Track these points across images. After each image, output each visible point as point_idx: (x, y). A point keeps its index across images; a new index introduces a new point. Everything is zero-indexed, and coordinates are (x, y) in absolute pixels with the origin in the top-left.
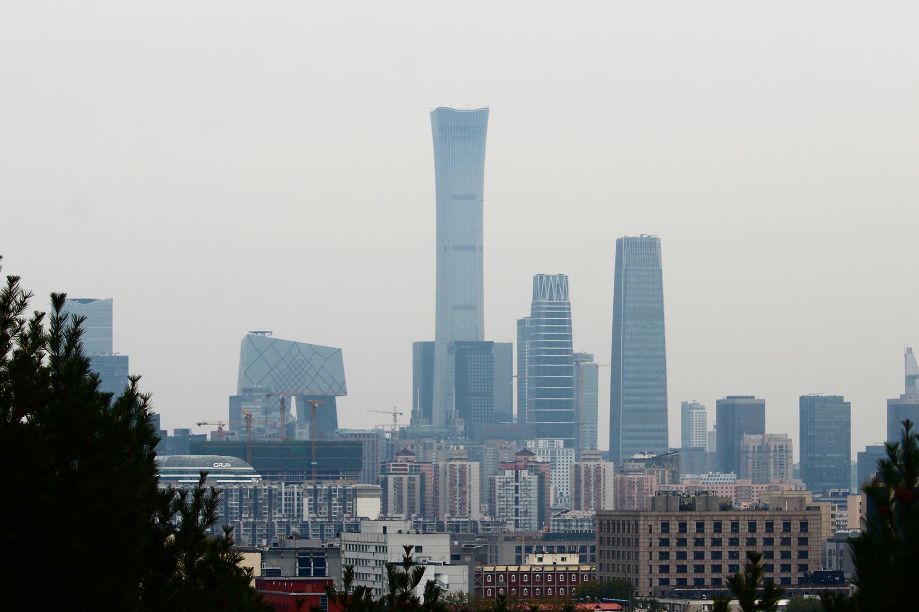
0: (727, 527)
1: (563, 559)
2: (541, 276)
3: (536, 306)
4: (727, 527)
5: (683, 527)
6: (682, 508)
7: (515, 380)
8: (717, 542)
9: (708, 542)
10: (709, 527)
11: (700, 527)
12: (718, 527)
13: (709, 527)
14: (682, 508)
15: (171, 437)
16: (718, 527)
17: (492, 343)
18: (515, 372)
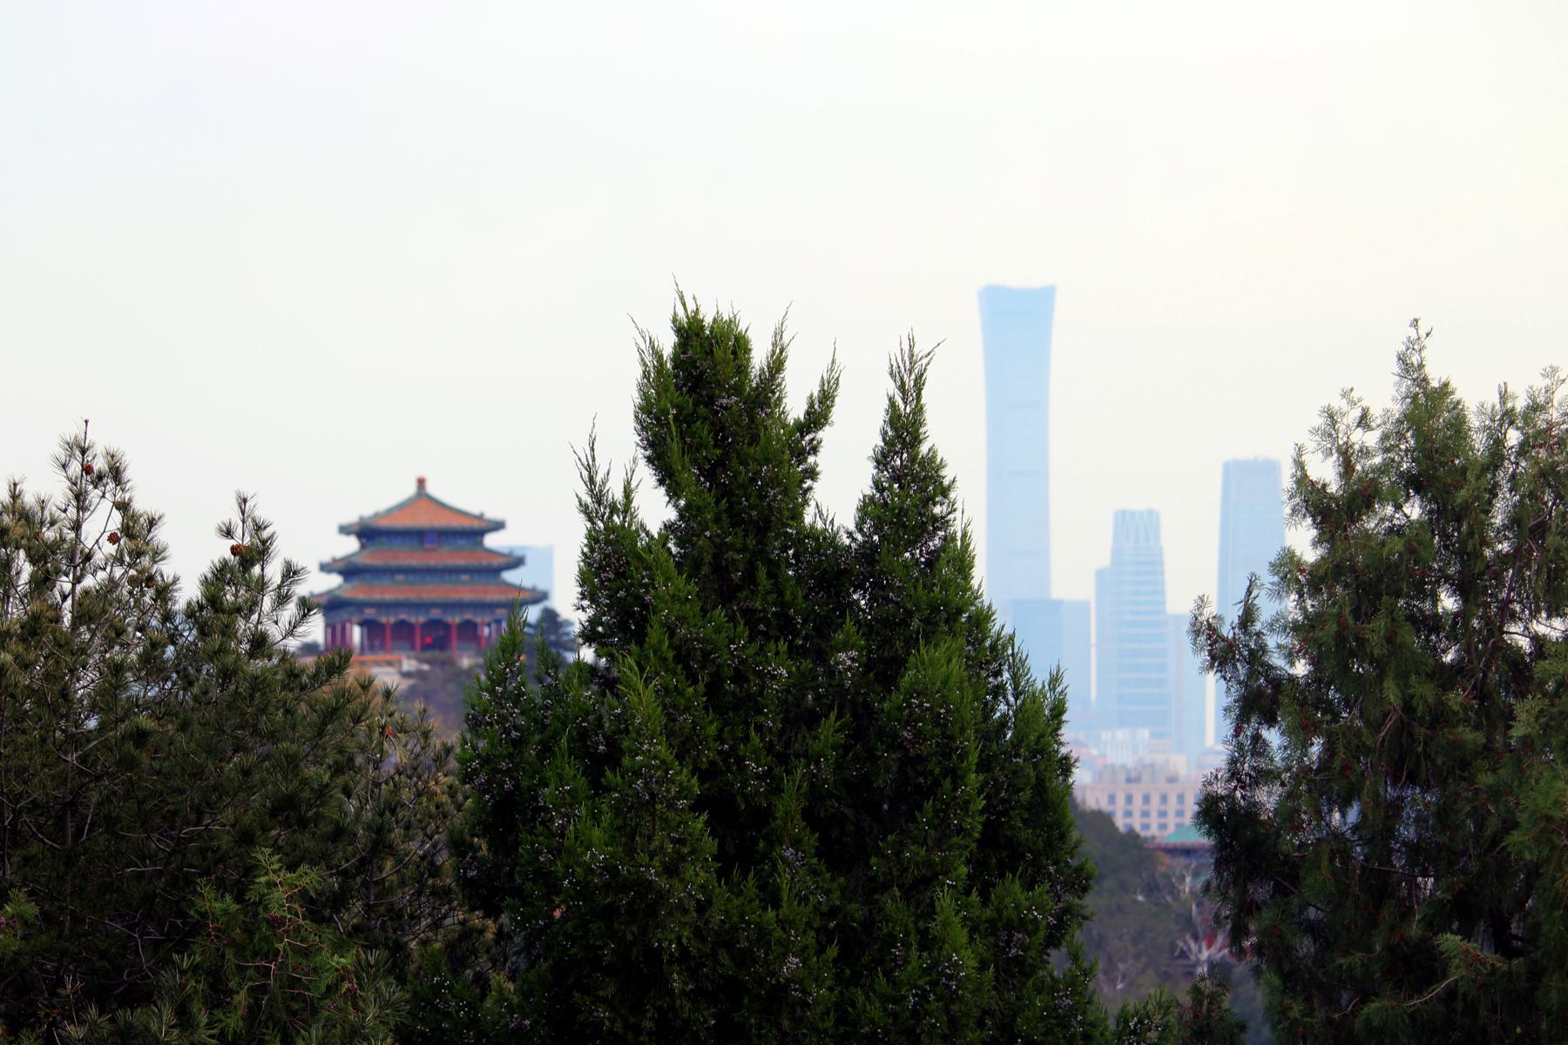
0: (1173, 799)
1: (888, 771)
2: (1123, 513)
3: (1117, 552)
4: (1173, 799)
5: (1129, 799)
6: (1129, 781)
7: (1093, 652)
8: (1163, 814)
9: (1154, 814)
10: (1155, 800)
11: (1146, 799)
12: (1164, 799)
13: (1155, 800)
14: (1129, 781)
15: (823, 541)
16: (1164, 799)
17: (1060, 603)
18: (1093, 640)
